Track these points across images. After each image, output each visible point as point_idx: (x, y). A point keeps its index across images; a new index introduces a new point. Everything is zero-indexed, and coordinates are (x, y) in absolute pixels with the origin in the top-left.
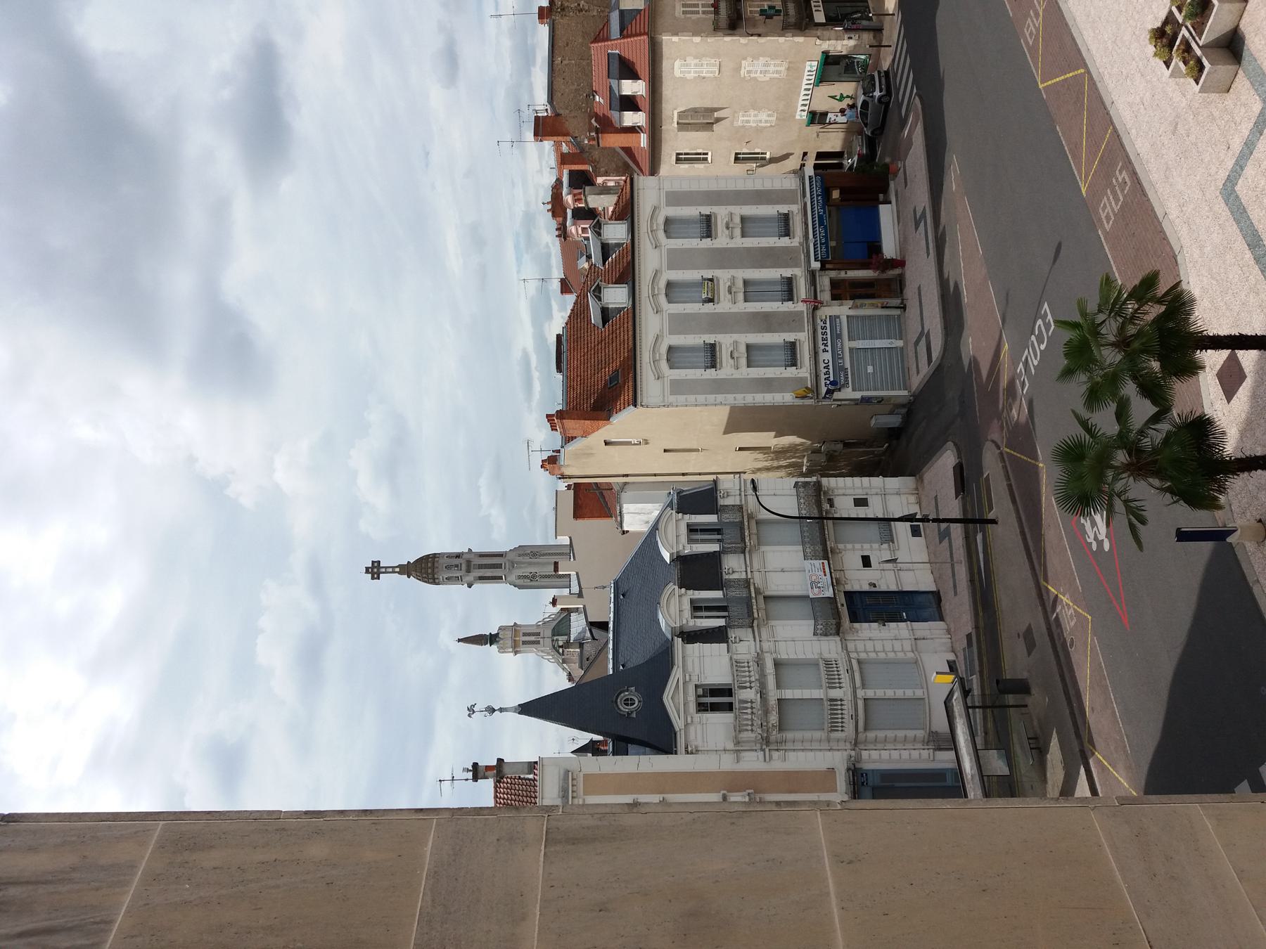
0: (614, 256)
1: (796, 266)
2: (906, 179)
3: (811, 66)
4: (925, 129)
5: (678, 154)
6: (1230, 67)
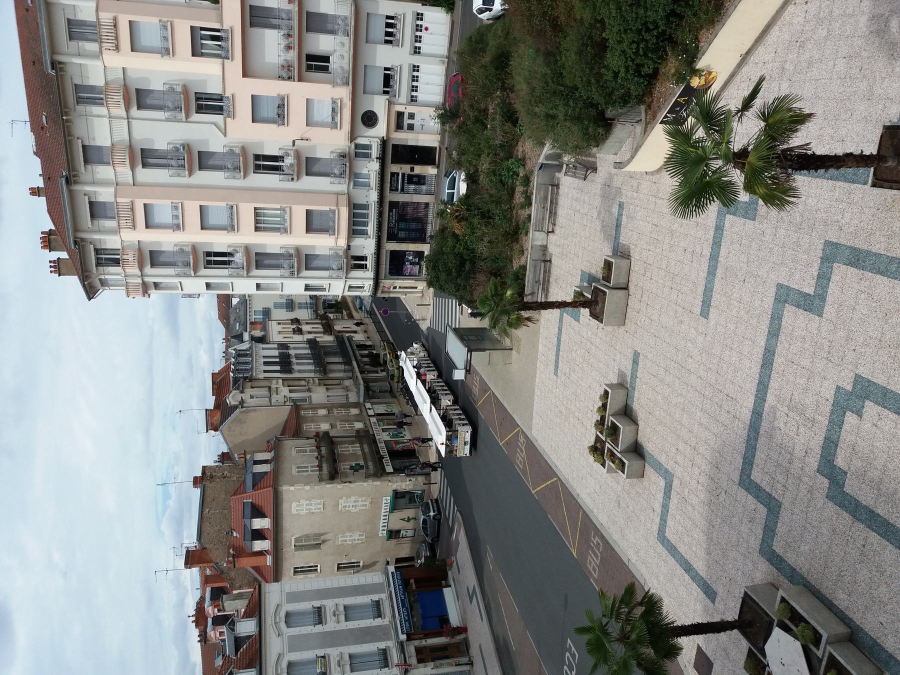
0: (245, 647)
1: (388, 639)
2: (458, 568)
3: (386, 500)
4: (466, 532)
5: (295, 568)
6: (640, 462)
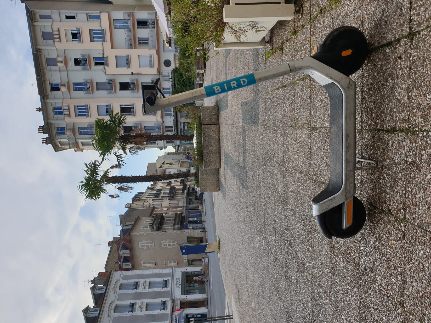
1: (168, 297)
